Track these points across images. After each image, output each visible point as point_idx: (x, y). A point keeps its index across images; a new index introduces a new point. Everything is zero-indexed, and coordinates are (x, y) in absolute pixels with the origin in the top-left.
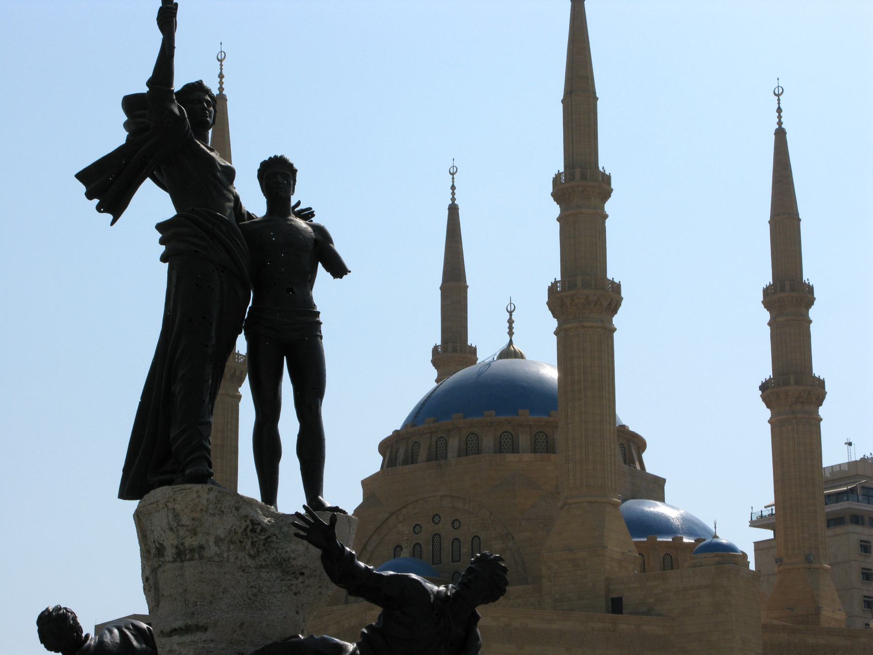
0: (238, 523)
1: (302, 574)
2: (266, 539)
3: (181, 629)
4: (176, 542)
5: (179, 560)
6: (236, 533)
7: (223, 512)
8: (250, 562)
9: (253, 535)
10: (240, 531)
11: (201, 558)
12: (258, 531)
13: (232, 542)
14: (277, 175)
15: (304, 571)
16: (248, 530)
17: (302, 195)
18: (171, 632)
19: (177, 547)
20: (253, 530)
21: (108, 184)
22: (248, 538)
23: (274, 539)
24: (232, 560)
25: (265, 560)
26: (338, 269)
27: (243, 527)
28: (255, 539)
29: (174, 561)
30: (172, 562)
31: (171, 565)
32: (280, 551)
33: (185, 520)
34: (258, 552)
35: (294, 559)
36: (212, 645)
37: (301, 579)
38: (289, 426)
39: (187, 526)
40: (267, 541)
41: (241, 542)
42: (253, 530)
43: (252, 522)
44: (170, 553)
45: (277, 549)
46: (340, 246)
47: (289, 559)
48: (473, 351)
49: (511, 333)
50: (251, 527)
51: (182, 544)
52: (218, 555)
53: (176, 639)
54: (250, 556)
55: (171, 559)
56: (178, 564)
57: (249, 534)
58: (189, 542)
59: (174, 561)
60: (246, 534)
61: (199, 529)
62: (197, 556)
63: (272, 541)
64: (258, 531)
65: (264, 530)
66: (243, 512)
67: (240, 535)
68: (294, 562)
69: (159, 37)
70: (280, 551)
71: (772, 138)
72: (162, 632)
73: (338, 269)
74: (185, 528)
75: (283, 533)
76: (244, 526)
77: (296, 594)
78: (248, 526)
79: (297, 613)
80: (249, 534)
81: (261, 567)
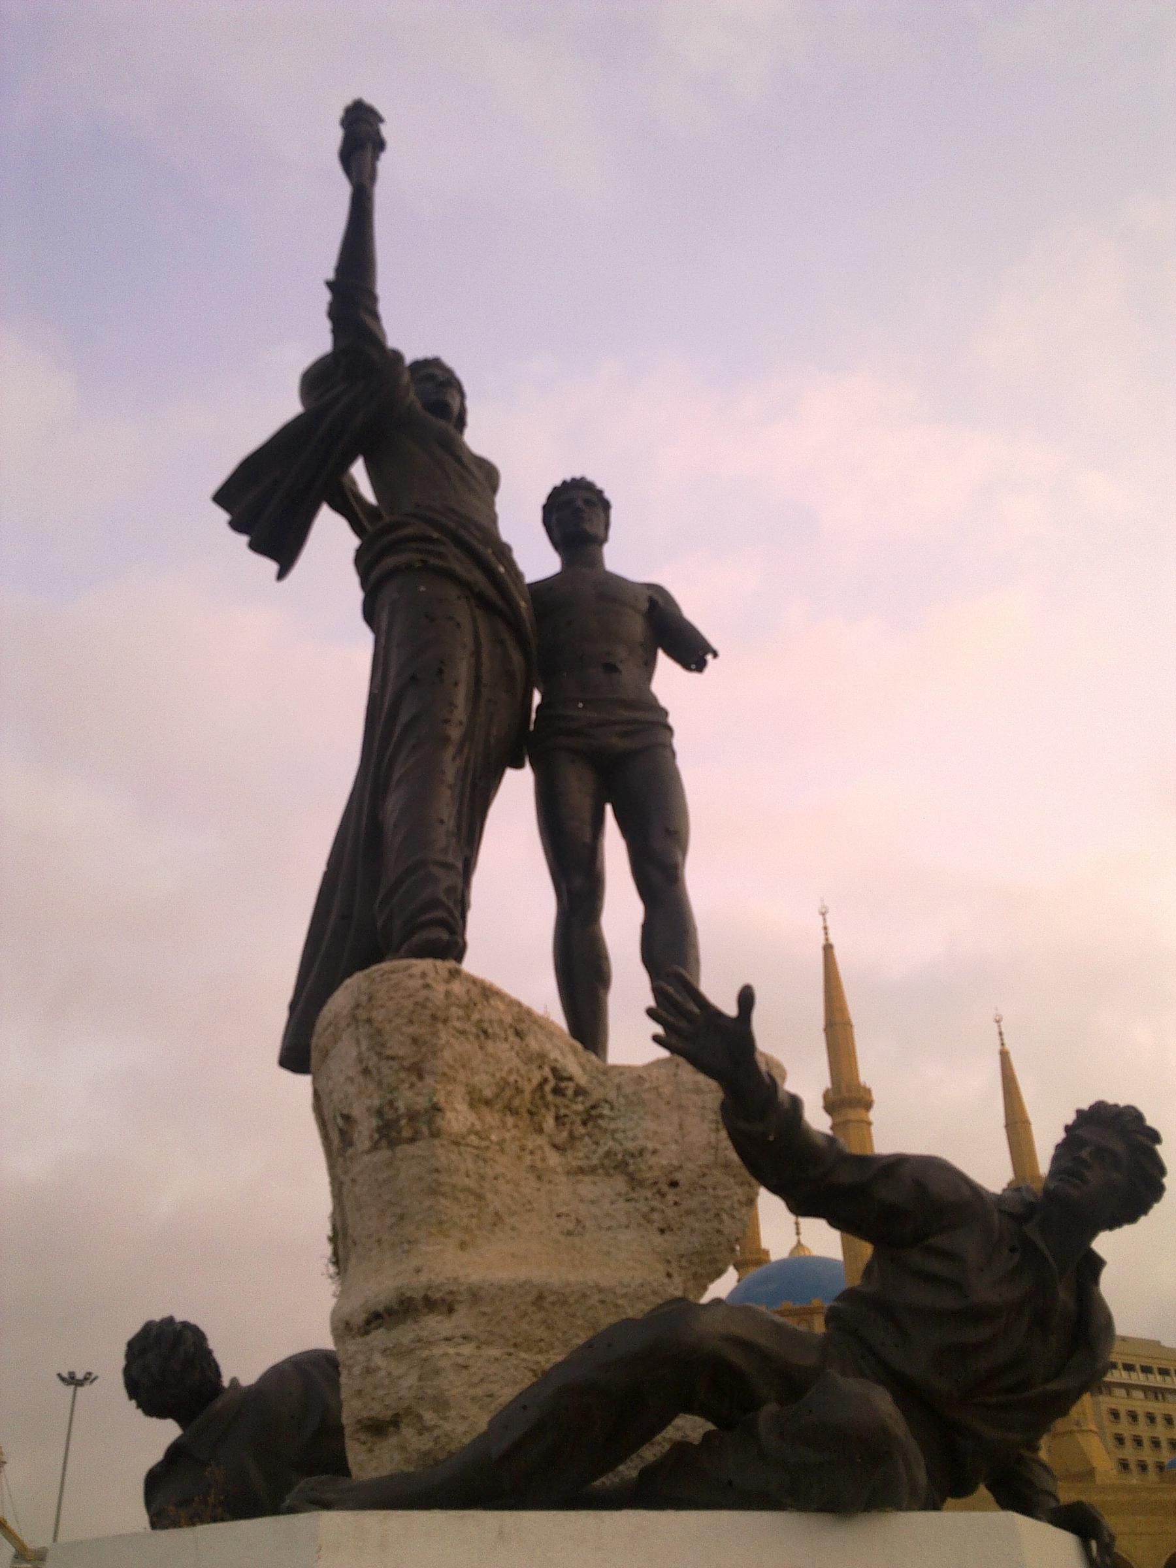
0: (523, 1069)
1: (674, 1184)
2: (587, 1112)
3: (390, 1311)
4: (376, 1102)
5: (384, 1143)
6: (519, 1091)
7: (485, 1032)
8: (554, 1159)
9: (559, 1100)
10: (528, 1088)
11: (435, 1134)
12: (570, 1092)
13: (510, 1109)
14: (576, 513)
15: (678, 1176)
16: (548, 1088)
17: (520, 445)
18: (368, 1322)
19: (380, 1113)
20: (557, 1091)
21: (268, 503)
22: (547, 1106)
23: (606, 1111)
24: (513, 1148)
25: (587, 1158)
26: (693, 652)
27: (535, 1082)
28: (563, 1111)
29: (375, 1147)
30: (368, 1152)
31: (366, 1158)
32: (619, 1136)
33: (397, 1046)
34: (572, 1137)
35: (654, 1152)
36: (468, 1349)
37: (671, 1197)
38: (622, 915)
39: (403, 1058)
40: (590, 1117)
41: (531, 1113)
42: (557, 1091)
43: (554, 1070)
44: (365, 1128)
45: (614, 1131)
46: (695, 610)
47: (641, 1153)
48: (767, 1253)
49: (798, 1234)
50: (552, 1083)
51: (391, 1103)
52: (477, 1133)
53: (379, 1337)
54: (556, 1147)
55: (367, 1144)
56: (384, 1154)
57: (550, 1097)
58: (406, 1099)
59: (375, 1147)
60: (543, 1097)
61: (427, 1066)
62: (425, 1130)
63: (601, 1116)
64: (570, 1092)
65: (580, 1091)
66: (533, 1044)
67: (527, 1095)
68: (653, 1160)
69: (343, 190)
70: (619, 1136)
71: (997, 1058)
72: (347, 1323)
73: (693, 652)
74: (395, 1064)
75: (626, 1097)
76: (537, 1077)
77: (662, 1231)
78: (545, 1080)
79: (669, 1275)
80: (550, 1097)
81: (581, 1170)
